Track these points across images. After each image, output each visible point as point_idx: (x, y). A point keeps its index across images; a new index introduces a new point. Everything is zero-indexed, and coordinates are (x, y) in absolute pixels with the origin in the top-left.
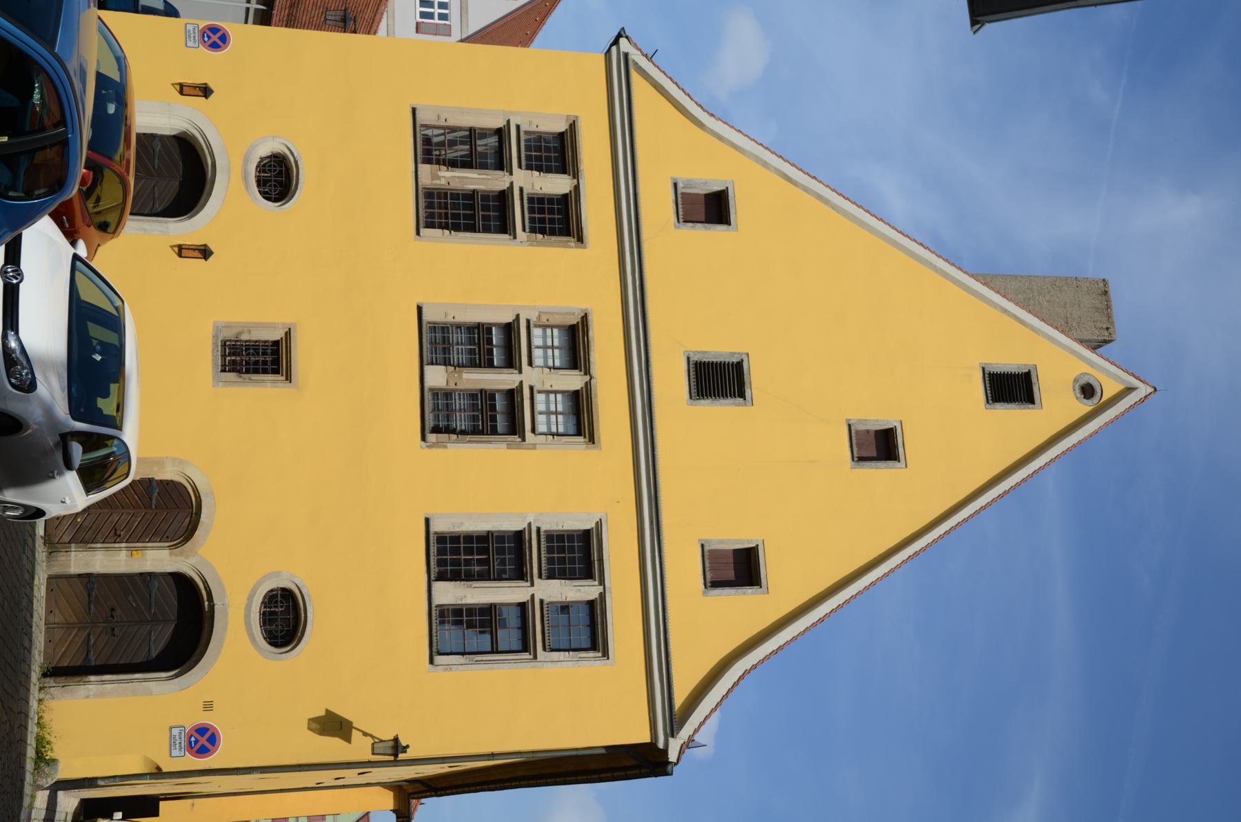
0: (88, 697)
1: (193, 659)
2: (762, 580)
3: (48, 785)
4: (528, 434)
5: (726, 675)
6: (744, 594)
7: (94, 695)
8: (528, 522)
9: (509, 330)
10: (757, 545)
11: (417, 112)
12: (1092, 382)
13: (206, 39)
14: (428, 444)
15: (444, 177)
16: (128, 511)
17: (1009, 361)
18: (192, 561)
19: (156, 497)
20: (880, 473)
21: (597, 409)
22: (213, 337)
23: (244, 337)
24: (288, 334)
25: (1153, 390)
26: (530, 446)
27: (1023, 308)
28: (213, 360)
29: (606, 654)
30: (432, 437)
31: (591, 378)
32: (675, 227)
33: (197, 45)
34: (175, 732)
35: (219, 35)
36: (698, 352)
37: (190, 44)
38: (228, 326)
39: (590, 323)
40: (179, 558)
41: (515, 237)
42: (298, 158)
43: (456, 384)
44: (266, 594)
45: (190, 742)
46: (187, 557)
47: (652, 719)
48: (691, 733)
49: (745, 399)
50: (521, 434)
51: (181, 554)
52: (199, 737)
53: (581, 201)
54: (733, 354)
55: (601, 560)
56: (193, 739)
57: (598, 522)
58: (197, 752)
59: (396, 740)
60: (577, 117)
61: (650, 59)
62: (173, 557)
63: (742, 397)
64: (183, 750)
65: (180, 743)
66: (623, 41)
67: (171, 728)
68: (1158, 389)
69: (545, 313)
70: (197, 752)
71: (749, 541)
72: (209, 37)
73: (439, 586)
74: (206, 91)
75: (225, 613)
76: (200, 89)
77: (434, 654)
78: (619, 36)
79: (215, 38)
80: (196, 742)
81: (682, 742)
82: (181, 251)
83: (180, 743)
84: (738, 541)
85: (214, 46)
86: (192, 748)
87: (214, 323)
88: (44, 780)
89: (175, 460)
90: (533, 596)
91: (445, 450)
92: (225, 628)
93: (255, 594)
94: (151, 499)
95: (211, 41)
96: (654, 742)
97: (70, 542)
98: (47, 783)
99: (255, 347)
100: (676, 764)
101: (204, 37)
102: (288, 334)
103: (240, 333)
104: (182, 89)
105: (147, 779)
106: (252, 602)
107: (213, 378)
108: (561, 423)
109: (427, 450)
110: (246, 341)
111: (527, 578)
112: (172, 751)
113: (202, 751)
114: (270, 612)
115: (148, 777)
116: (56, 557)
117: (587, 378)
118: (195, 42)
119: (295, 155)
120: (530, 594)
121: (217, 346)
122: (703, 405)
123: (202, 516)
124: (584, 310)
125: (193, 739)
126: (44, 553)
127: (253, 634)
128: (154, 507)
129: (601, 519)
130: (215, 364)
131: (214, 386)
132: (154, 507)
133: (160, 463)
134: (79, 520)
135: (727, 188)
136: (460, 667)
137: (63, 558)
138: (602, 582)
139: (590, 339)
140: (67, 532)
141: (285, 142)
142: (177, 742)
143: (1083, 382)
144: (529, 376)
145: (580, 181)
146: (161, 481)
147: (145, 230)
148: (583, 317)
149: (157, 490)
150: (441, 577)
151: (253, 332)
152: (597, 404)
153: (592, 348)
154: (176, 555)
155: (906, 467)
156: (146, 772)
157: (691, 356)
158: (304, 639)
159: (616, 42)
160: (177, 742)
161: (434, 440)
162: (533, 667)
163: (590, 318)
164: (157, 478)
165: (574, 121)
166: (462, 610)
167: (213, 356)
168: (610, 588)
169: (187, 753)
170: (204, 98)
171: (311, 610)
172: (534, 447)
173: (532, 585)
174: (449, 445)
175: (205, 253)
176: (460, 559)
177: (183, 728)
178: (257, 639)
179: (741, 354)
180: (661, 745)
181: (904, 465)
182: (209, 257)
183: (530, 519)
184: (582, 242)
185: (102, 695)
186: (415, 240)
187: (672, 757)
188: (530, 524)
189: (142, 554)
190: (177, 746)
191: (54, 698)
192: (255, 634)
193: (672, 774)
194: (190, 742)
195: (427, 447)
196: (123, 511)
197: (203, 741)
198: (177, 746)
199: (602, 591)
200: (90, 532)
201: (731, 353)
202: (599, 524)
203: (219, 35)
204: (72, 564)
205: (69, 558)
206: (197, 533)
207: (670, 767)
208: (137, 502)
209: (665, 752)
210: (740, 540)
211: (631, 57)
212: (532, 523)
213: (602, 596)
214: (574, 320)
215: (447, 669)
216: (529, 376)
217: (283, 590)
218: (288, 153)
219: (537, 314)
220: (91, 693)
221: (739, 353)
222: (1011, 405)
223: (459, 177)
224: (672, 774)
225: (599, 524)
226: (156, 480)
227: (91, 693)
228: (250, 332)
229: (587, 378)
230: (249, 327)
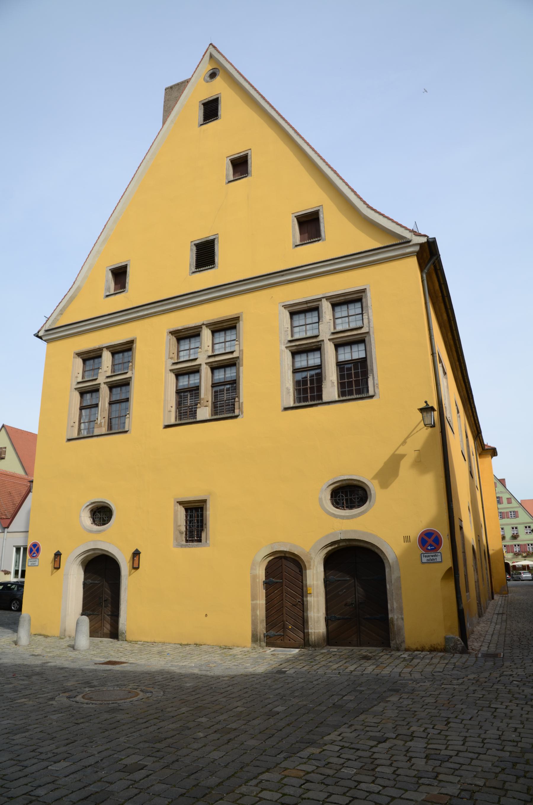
0: (402, 619)
1: (376, 550)
2: (315, 210)
3: (463, 643)
4: (235, 355)
5: (371, 218)
6: (323, 218)
7: (401, 615)
8: (285, 349)
9: (178, 374)
10: (295, 216)
11: (69, 438)
12: (208, 75)
13: (35, 555)
14: (240, 414)
15: (100, 420)
16: (284, 596)
17: (198, 113)
18: (313, 555)
19: (276, 579)
20: (254, 164)
21: (135, 352)
22: (182, 547)
23: (183, 529)
24: (180, 503)
25: (211, 46)
26: (241, 353)
27: (170, 113)
28: (194, 547)
29: (364, 291)
30: (237, 412)
31: (203, 324)
32: (127, 292)
33: (37, 560)
34: (425, 560)
35: (33, 548)
36: (190, 268)
37: (37, 564)
38: (176, 539)
39: (175, 329)
40: (312, 563)
41: (131, 378)
42: (90, 502)
43: (207, 401)
44: (335, 507)
45: (431, 550)
46: (311, 558)
47: (402, 257)
48: (408, 231)
49: (215, 239)
50: (235, 360)
51: (309, 562)
52: (428, 544)
53: (113, 344)
54: (191, 250)
55: (307, 302)
56: (429, 548)
57: (284, 308)
58: (438, 545)
59: (422, 410)
60: (74, 353)
61: (49, 319)
62: (312, 567)
63: (214, 241)
64: (437, 554)
65: (432, 556)
66: (40, 334)
67: (423, 563)
68: (210, 43)
69: (169, 355)
70: (438, 545)
71: (293, 221)
72: (34, 553)
73: (326, 397)
74: (58, 555)
75: (346, 532)
76: (57, 558)
77: (368, 396)
78: (37, 336)
79: (34, 550)
80: (431, 545)
81: (413, 236)
82: (136, 568)
83: (432, 556)
84: (293, 227)
85: (38, 550)
86: (435, 548)
87: (174, 547)
88: (459, 646)
89: (252, 569)
90: (329, 340)
91: (244, 403)
92: (355, 531)
93: (333, 514)
94: (277, 582)
95: (36, 552)
96: (416, 254)
97: (304, 633)
98: (461, 644)
99: (189, 520)
100: (428, 237)
101: (34, 556)
102: (180, 503)
103: (181, 533)
104: (57, 568)
105: (297, 395)
106: (338, 515)
107: (204, 546)
108: (230, 335)
109: (244, 414)
110: (186, 528)
111: (319, 345)
112: (437, 561)
113: (437, 541)
114: (347, 503)
115: (457, 576)
116: (312, 641)
117: (204, 327)
118: (36, 561)
119: (88, 504)
120: (328, 341)
121: (187, 545)
122: (218, 260)
123: (285, 550)
124: (168, 334)
125: (429, 548)
126: (310, 649)
127: (359, 513)
128: (281, 581)
129: (283, 306)
130: (197, 546)
131: (209, 546)
132: (281, 581)
133: (254, 578)
134: (290, 627)
135: (110, 270)
136: (376, 378)
137: (313, 637)
138: (320, 300)
139: (183, 328)
140: (298, 635)
141: (84, 507)
142: (432, 558)
143: (208, 79)
144: (202, 359)
145: (104, 346)
146: (266, 577)
147: (125, 588)
148: (172, 334)
149: (271, 579)
150: (320, 397)
151: (179, 524)
152: (218, 318)
153: (187, 326)
154: (310, 565)
155: (250, 149)
156: (453, 578)
157: (191, 272)
158: (361, 480)
159: (40, 338)
160: (432, 558)
161: (238, 410)
162: (373, 333)
163: (171, 330)
164: (264, 579)
165: (76, 354)
166: (341, 383)
167: (192, 547)
168: (323, 294)
169: (438, 551)
170: (62, 556)
171: (343, 477)
172: (241, 351)
173: (323, 341)
174: (241, 401)
175: (136, 554)
176: (310, 388)
177: (422, 555)
178: (362, 510)
179: (191, 245)
180: (417, 248)
181: (250, 151)
182: (139, 551)
183: (283, 347)
184: (133, 340)
185: (401, 610)
186: (130, 433)
187: (423, 240)
188: (287, 347)
189: (310, 587)
190: (434, 558)
191: (404, 641)
192: (359, 512)
193: (435, 238)
194: (431, 550)
195: (242, 413)
196: (284, 600)
197: (430, 541)
198: (434, 558)
199: (325, 299)
200: (298, 621)
201: (190, 250)
202: (285, 307)
203: (33, 548)
204: (317, 631)
205: (313, 634)
206: (296, 553)
207: (430, 240)
208: (278, 591)
209: (421, 245)
210: (292, 226)
211: (47, 329)
212: (286, 346)
213: (328, 298)
214: (174, 340)
215: (377, 387)
216: (202, 359)
217: (332, 497)
218: (90, 506)
219: (170, 360)
220: (400, 616)
221: (191, 247)
222: (219, 108)
223: (101, 412)
224: (435, 238)
225: (285, 307)
226: (266, 579)
227: (400, 616)
228: (180, 526)
229: (204, 327)
230: (177, 526)
